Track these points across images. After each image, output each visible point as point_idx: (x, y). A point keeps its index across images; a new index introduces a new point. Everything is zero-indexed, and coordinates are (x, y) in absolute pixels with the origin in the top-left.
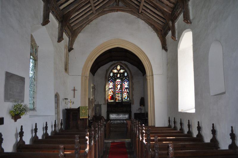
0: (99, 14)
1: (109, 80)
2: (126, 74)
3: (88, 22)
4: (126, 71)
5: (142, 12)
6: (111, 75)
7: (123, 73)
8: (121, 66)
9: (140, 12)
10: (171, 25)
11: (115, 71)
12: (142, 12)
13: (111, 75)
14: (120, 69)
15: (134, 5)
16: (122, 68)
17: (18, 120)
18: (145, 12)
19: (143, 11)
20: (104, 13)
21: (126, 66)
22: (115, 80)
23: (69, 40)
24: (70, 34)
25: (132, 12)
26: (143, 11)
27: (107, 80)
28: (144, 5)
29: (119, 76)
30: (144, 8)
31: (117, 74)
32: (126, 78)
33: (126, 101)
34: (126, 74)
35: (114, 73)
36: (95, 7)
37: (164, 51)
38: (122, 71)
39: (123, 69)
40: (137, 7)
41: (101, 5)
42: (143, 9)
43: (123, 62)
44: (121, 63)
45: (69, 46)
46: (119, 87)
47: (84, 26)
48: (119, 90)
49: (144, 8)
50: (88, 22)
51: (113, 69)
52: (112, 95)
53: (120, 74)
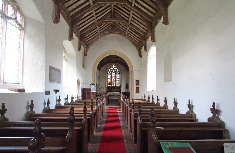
0: (102, 35)
1: (108, 74)
2: (118, 70)
3: (95, 40)
4: (118, 69)
5: (127, 35)
6: (109, 70)
7: (116, 70)
8: (115, 66)
9: (126, 35)
10: (144, 43)
11: (112, 68)
12: (127, 35)
13: (109, 70)
14: (115, 68)
15: (122, 30)
16: (115, 67)
17: (58, 93)
18: (129, 35)
19: (128, 34)
20: (105, 34)
21: (118, 66)
22: (111, 74)
23: (85, 50)
24: (85, 46)
25: (122, 35)
26: (128, 34)
27: (107, 74)
28: (129, 31)
29: (114, 71)
30: (129, 32)
31: (113, 70)
32: (118, 73)
33: (118, 85)
34: (118, 70)
35: (111, 70)
36: (100, 30)
37: (140, 57)
38: (116, 69)
39: (117, 67)
40: (125, 32)
41: (103, 30)
42: (128, 33)
43: (116, 63)
44: (115, 64)
45: (85, 53)
46: (114, 77)
47: (93, 42)
48: (114, 79)
49: (129, 32)
50: (95, 40)
51: (111, 67)
52: (110, 82)
53: (115, 70)
